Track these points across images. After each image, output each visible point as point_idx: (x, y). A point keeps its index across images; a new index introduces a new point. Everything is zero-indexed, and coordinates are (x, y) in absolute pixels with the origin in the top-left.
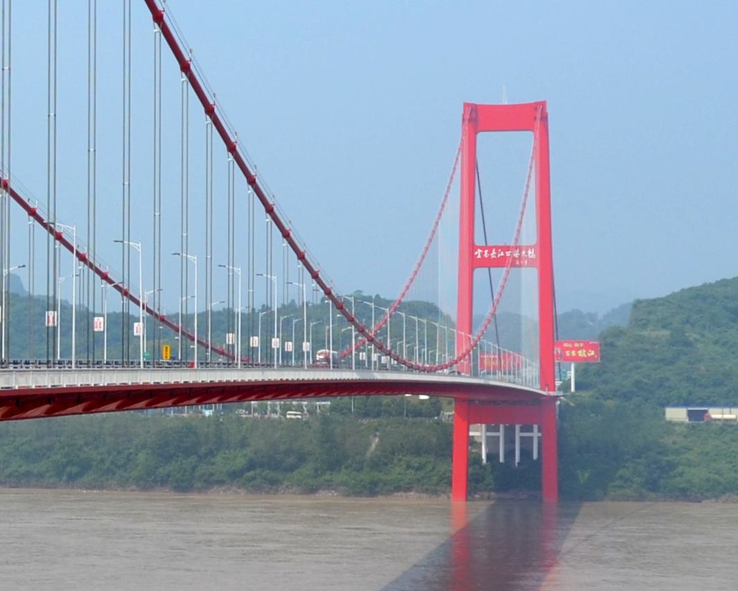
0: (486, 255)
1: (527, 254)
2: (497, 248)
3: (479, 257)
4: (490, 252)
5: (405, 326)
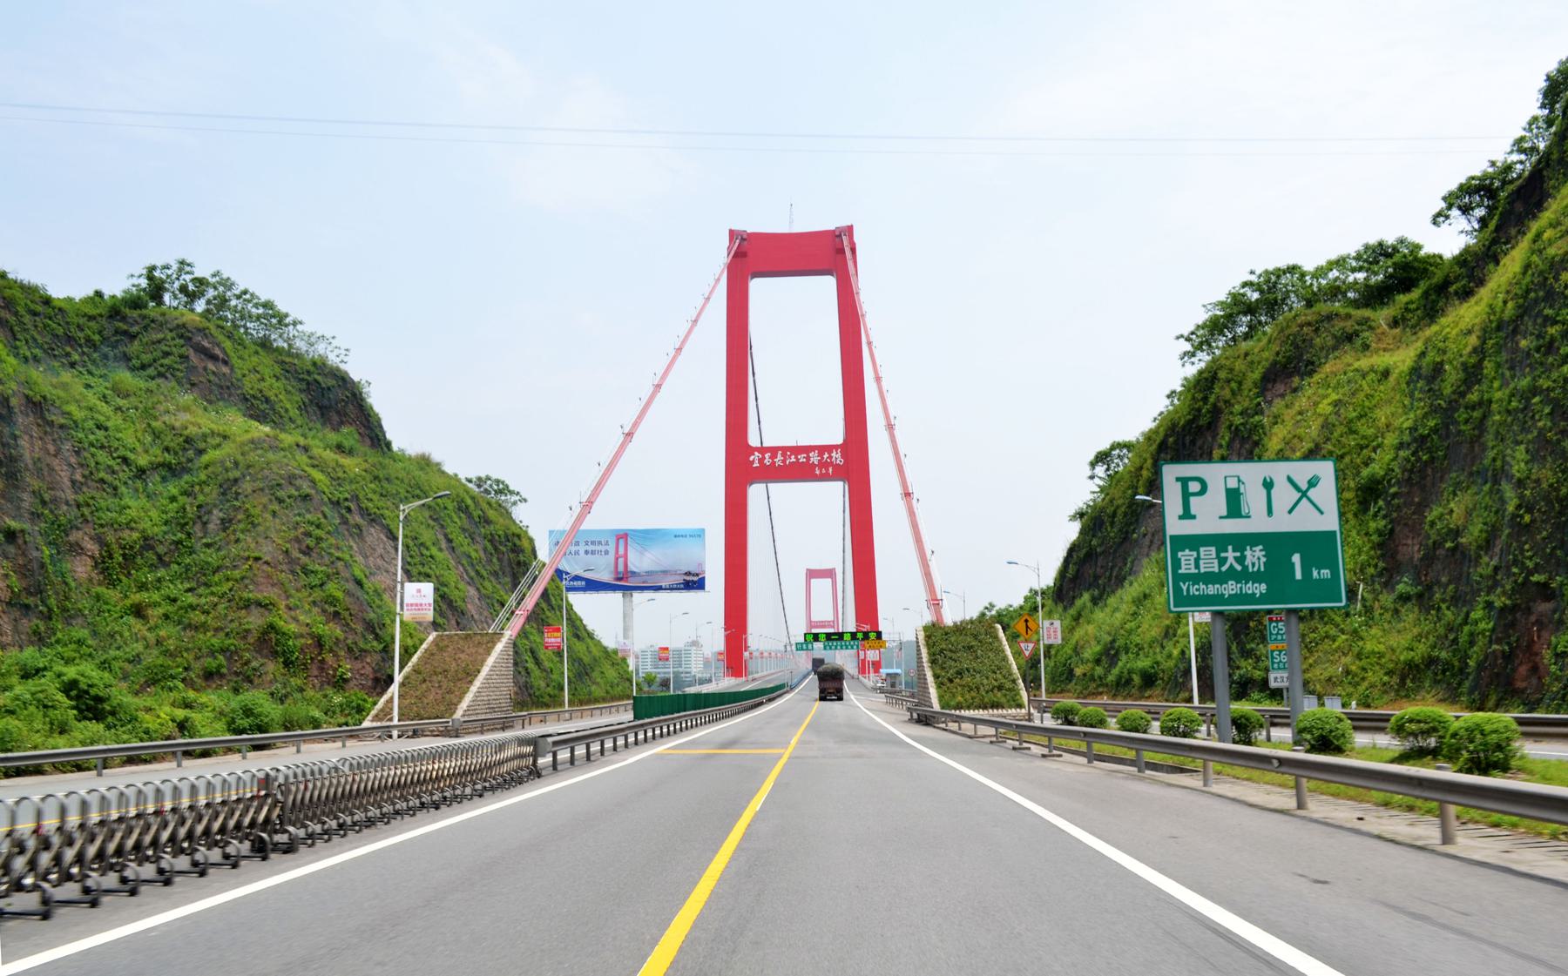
0: (767, 461)
1: (830, 457)
2: (784, 449)
3: (756, 464)
4: (773, 457)
5: (491, 661)
